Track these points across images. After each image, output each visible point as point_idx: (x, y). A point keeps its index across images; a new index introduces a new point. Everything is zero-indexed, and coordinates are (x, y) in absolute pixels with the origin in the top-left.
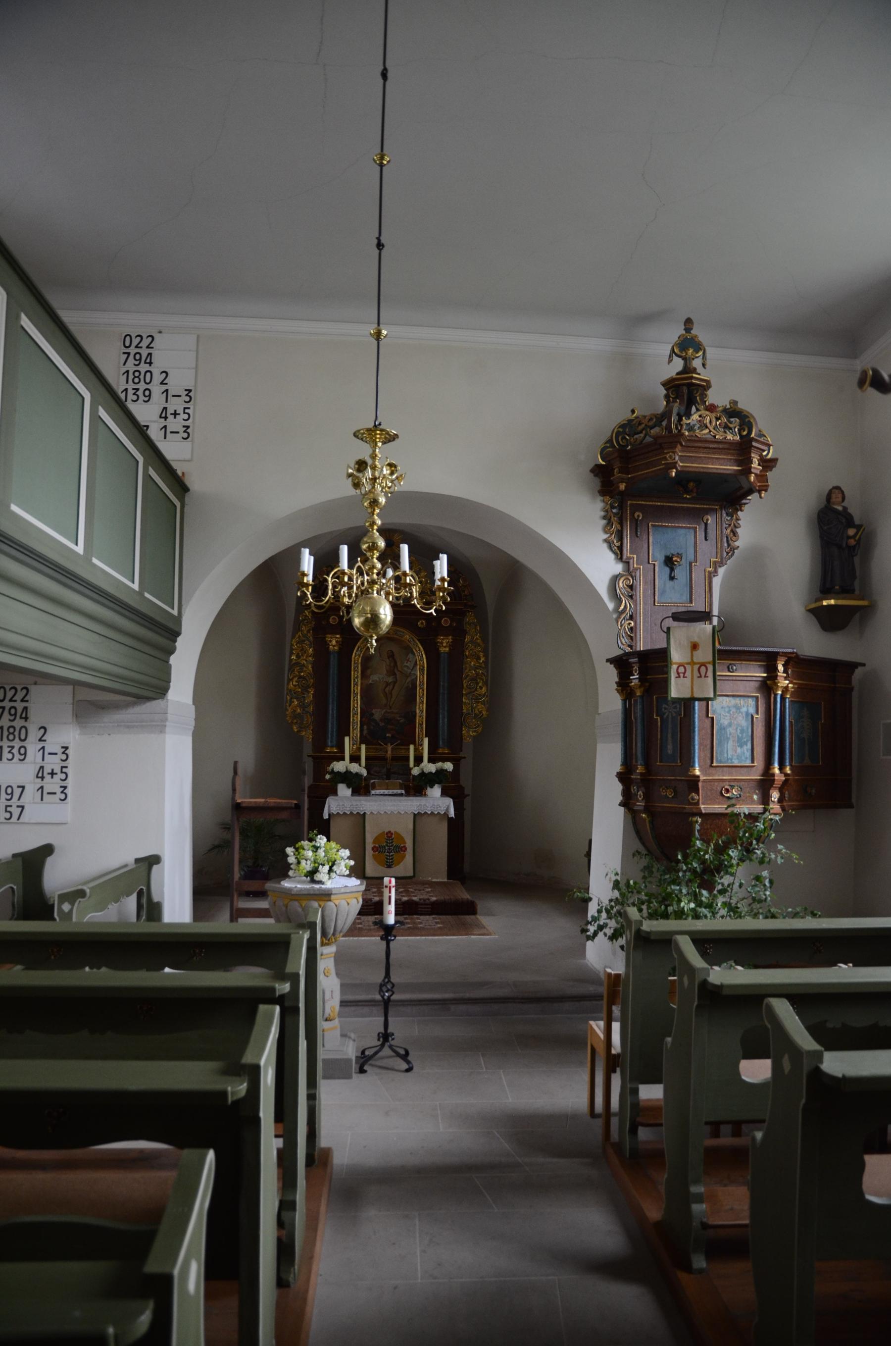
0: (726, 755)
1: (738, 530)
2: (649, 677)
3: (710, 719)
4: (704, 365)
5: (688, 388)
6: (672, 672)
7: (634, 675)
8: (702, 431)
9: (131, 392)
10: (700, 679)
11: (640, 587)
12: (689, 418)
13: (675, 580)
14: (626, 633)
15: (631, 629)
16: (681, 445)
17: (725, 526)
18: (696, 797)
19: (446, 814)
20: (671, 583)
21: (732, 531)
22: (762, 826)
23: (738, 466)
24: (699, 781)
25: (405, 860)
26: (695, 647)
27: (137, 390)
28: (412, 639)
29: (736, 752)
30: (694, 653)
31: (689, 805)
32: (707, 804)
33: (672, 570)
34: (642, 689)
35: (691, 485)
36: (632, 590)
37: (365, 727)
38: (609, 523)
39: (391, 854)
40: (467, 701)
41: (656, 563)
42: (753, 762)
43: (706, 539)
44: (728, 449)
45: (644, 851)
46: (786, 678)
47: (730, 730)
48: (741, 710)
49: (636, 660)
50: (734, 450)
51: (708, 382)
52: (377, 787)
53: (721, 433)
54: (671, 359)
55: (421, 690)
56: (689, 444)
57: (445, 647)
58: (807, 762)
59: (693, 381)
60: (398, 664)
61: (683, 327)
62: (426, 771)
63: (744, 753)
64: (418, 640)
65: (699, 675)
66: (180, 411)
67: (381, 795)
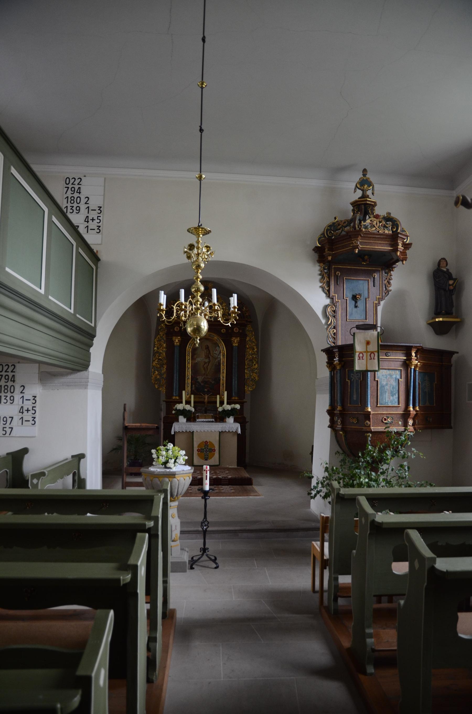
0: (384, 401)
1: (391, 281)
2: (344, 359)
3: (376, 382)
4: (373, 194)
5: (365, 206)
6: (356, 356)
7: (336, 358)
8: (372, 228)
9: (69, 208)
10: (371, 360)
11: (339, 312)
12: (365, 222)
13: (357, 308)
14: (332, 336)
15: (334, 334)
16: (361, 236)
17: (384, 279)
18: (369, 423)
19: (236, 432)
20: (356, 309)
21: (388, 282)
22: (404, 438)
23: (391, 247)
24: (370, 414)
25: (214, 456)
26: (368, 343)
27: (73, 207)
28: (218, 339)
29: (390, 399)
30: (368, 346)
31: (365, 427)
32: (375, 427)
33: (356, 302)
34: (340, 366)
35: (366, 257)
36: (335, 313)
37: (193, 386)
38: (323, 278)
39: (207, 453)
40: (247, 372)
41: (347, 299)
42: (399, 404)
43: (374, 286)
44: (385, 238)
45: (341, 452)
46: (416, 360)
47: (387, 387)
48: (393, 377)
49: (337, 350)
50: (389, 239)
51: (375, 202)
52: (200, 418)
53: (382, 230)
54: (356, 190)
55: (223, 366)
56: (365, 236)
57: (236, 343)
58: (427, 404)
59: (367, 202)
60: (211, 352)
61: (362, 174)
62: (226, 409)
63: (394, 399)
64: (221, 339)
65: (370, 358)
66: (95, 218)
67: (202, 422)
